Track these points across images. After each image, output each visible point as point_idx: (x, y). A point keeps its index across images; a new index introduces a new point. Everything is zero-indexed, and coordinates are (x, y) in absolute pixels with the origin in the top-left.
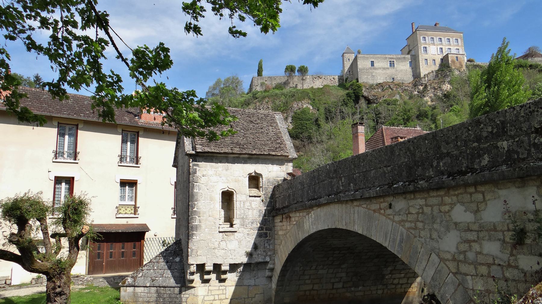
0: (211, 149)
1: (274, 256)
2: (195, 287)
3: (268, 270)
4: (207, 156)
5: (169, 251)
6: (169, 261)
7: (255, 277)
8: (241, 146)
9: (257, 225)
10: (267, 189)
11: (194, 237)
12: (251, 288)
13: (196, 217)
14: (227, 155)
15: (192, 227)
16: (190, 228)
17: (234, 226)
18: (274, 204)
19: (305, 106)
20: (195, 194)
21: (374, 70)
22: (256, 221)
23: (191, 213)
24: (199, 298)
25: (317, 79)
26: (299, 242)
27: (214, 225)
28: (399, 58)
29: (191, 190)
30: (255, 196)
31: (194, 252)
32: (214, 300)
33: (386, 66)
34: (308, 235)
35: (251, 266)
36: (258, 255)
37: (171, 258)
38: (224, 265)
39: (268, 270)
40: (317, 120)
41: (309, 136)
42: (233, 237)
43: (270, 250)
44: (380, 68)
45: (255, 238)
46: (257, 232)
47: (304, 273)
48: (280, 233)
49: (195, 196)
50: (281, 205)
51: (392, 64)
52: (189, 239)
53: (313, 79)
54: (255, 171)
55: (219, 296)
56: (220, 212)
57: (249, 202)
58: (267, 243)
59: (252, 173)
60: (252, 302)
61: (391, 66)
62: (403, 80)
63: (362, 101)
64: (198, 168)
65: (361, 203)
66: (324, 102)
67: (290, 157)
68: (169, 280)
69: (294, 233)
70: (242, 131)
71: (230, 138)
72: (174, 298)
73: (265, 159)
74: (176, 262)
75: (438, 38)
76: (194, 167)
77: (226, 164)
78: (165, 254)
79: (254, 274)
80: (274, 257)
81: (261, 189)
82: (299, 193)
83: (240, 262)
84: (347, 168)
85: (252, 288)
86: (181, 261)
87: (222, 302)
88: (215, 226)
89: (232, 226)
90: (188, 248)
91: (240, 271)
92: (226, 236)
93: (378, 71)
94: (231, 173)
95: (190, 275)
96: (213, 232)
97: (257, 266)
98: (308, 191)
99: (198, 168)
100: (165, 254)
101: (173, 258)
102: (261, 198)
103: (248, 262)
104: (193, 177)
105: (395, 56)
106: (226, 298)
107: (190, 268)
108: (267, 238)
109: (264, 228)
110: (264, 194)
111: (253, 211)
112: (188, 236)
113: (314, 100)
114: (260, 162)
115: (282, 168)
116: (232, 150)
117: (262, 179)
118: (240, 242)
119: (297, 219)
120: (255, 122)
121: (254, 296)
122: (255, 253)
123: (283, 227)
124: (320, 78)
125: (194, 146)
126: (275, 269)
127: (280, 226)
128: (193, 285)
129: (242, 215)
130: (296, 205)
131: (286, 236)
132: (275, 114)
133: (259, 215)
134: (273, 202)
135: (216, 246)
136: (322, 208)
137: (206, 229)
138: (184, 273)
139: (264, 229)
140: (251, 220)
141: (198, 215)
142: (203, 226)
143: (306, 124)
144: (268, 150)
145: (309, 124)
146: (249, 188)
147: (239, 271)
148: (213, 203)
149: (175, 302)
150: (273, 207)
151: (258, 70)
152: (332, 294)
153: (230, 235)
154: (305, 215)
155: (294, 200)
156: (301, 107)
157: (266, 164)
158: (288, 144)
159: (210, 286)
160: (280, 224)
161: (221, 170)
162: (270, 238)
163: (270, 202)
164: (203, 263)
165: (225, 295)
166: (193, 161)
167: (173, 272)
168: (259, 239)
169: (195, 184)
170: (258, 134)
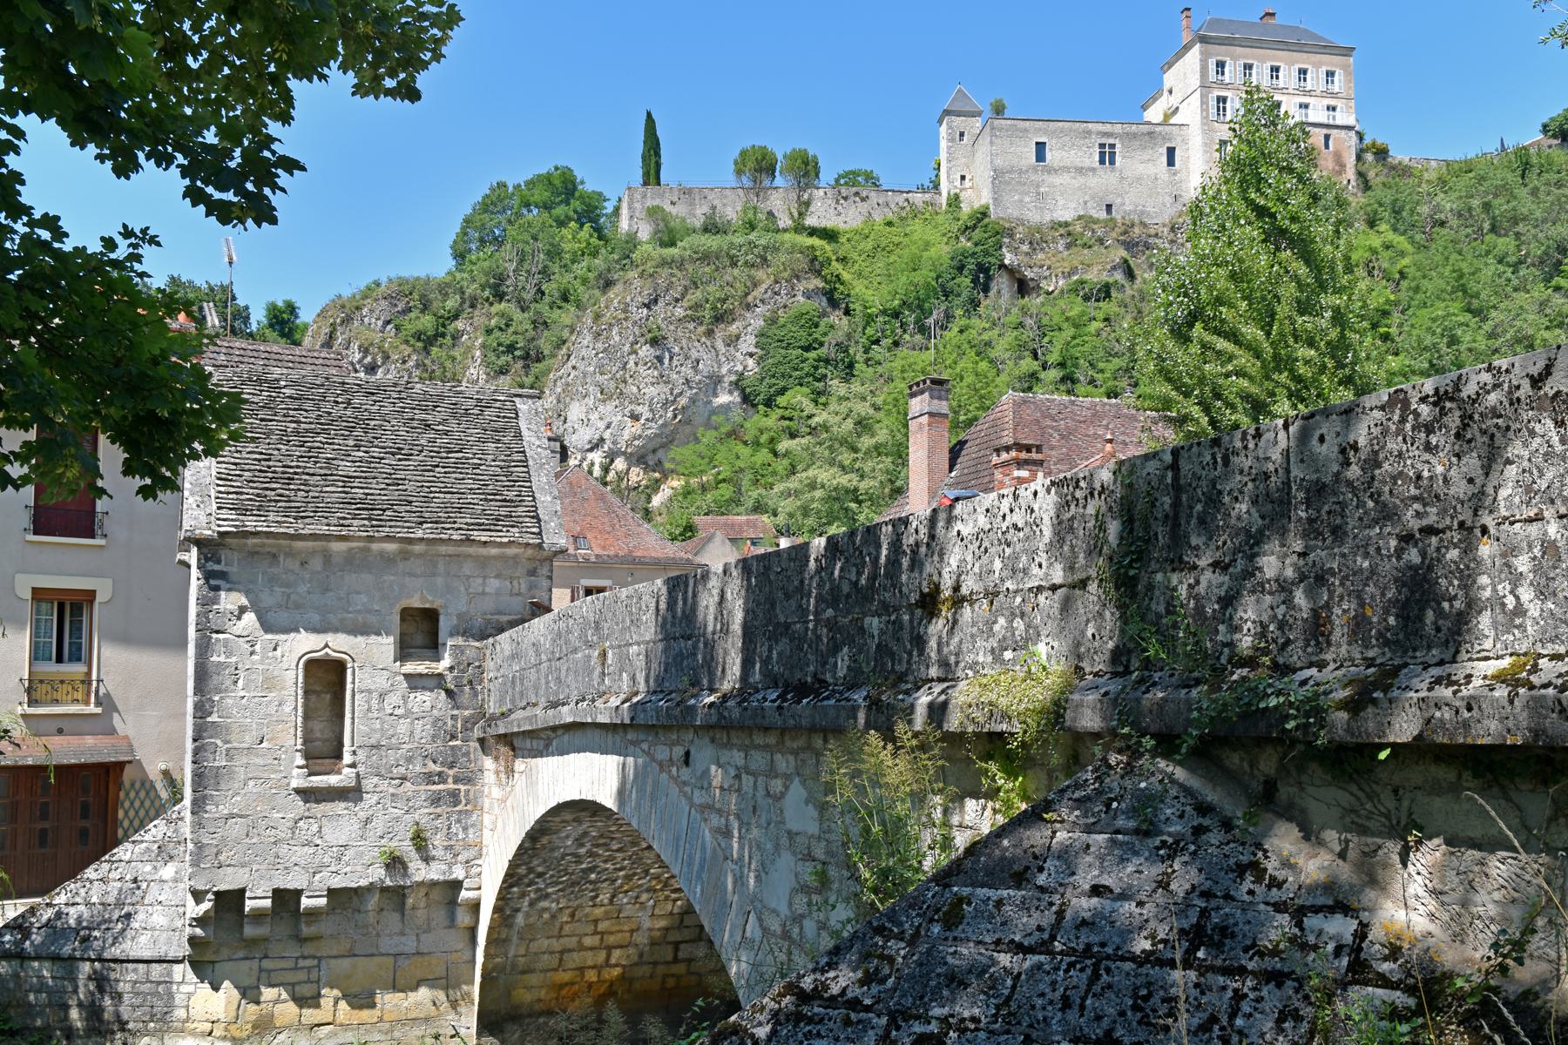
10: (462, 653)
11: (208, 808)
21: (1046, 176)
28: (1135, 136)
33: (1087, 163)
44: (1066, 169)
49: (215, 677)
51: (1107, 156)
58: (459, 821)
61: (1102, 162)
62: (1142, 212)
63: (1001, 283)
65: (642, 737)
75: (1269, 64)
84: (617, 624)
85: (407, 962)
93: (1057, 180)
105: (1118, 129)
109: (448, 776)
124: (863, 200)
132: (517, 400)
136: (571, 733)
139: (450, 780)
152: (673, 975)
162: (469, 807)
165: (315, 985)
168: (431, 810)
169: (214, 636)
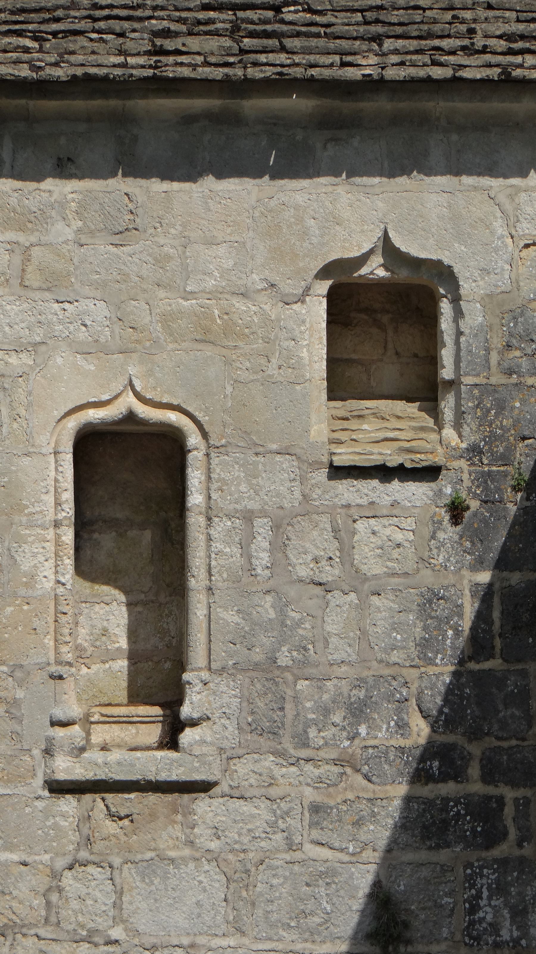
14: (113, 103)
22: (389, 697)
42: (177, 831)
45: (389, 850)
57: (325, 521)
59: (364, 259)
88: (16, 736)
108: (497, 852)
109: (467, 758)
116: (162, 52)
117: (458, 314)
153: (153, 816)
161: (69, 234)
168: (423, 855)
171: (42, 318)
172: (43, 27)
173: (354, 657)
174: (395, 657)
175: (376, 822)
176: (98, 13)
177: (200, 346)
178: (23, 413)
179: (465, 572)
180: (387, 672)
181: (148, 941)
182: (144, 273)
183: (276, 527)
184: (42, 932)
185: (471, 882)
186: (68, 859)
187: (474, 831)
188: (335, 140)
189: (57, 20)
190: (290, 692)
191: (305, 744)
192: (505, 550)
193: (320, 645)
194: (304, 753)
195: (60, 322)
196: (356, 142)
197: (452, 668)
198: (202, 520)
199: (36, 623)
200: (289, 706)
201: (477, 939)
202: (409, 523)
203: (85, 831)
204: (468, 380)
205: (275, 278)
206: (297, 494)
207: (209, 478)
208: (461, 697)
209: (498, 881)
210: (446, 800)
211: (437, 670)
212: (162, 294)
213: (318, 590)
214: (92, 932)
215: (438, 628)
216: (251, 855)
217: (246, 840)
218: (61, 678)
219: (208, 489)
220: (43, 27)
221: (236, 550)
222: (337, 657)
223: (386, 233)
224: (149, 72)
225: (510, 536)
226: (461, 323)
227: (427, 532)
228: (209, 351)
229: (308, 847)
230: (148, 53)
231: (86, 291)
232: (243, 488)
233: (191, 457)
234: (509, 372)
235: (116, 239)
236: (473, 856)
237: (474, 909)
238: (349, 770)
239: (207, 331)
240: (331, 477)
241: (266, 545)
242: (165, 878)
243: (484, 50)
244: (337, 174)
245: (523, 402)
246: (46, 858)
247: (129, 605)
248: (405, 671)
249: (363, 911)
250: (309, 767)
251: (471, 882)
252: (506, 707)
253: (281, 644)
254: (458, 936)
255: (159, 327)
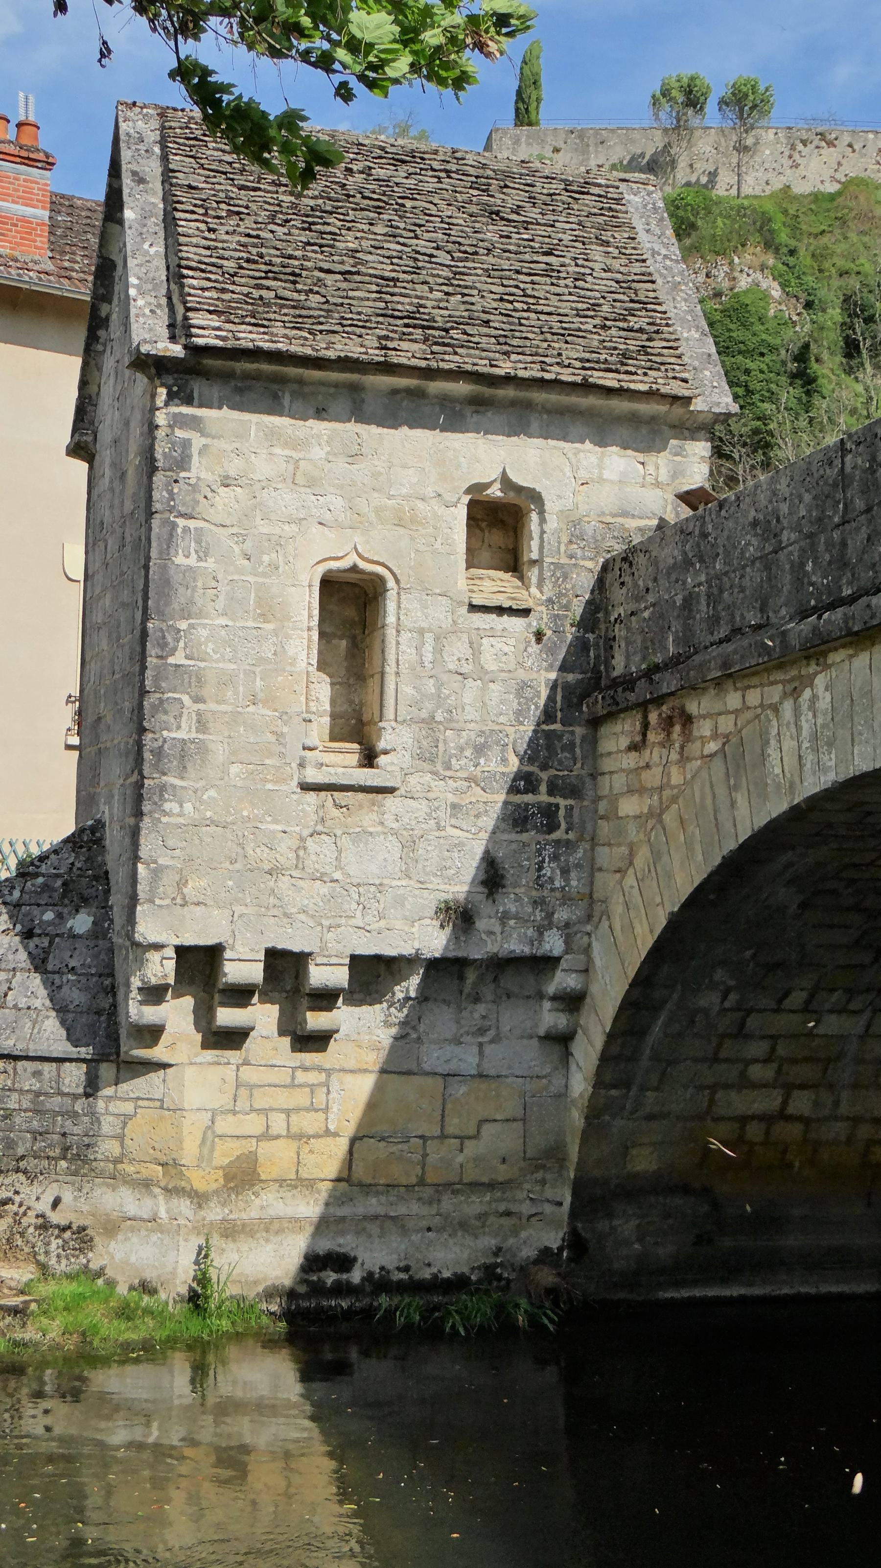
0: (272, 334)
1: (589, 928)
2: (170, 1066)
3: (554, 998)
4: (246, 376)
5: (40, 880)
6: (37, 931)
7: (482, 1031)
8: (436, 333)
9: (504, 760)
10: (565, 577)
11: (167, 806)
12: (460, 1090)
13: (179, 700)
15: (158, 753)
16: (147, 755)
17: (382, 760)
18: (597, 657)
19: (744, 283)
20: (176, 578)
22: (497, 743)
23: (157, 679)
24: (186, 1123)
25: (811, 147)
26: (731, 845)
27: (278, 749)
29: (161, 553)
30: (500, 610)
31: (168, 881)
32: (266, 1136)
34: (784, 806)
35: (462, 978)
36: (504, 918)
37: (49, 916)
38: (325, 960)
39: (554, 998)
40: (802, 355)
41: (756, 432)
42: (374, 816)
43: (567, 899)
45: (494, 833)
46: (501, 797)
47: (742, 1024)
48: (629, 807)
49: (181, 590)
50: (637, 658)
52: (139, 814)
53: (793, 147)
54: (504, 473)
55: (294, 1118)
56: (309, 682)
57: (465, 637)
58: (555, 858)
60: (460, 1159)
64: (197, 441)
66: (840, 263)
67: (698, 405)
68: (35, 1022)
69: (709, 801)
70: (443, 257)
71: (374, 288)
72: (57, 1113)
73: (561, 412)
74: (75, 936)
76: (179, 433)
77: (352, 427)
78: (16, 894)
79: (476, 1015)
80: (589, 934)
81: (533, 575)
82: (746, 582)
83: (407, 950)
85: (463, 1089)
86: (99, 932)
87: (306, 1149)
89: (369, 758)
90: (136, 858)
91: (408, 999)
92: (335, 812)
94: (376, 475)
95: (142, 1003)
96: (269, 786)
97: (495, 980)
98: (802, 565)
99: (197, 441)
100: (16, 894)
101: (60, 916)
102: (533, 621)
103: (450, 955)
104: (168, 484)
106: (328, 1133)
107: (141, 963)
108: (555, 836)
109: (539, 781)
110: (550, 601)
111: (484, 689)
112: (139, 798)
113: (792, 252)
114: (535, 425)
115: (651, 469)
117: (543, 520)
118: (409, 845)
119: (726, 724)
120: (514, 217)
121: (472, 1131)
122: (485, 908)
123: (645, 775)
124: (831, 144)
125: (179, 318)
126: (588, 1000)
127: (629, 772)
128: (158, 1053)
129: (429, 706)
130: (729, 648)
131: (660, 821)
132: (623, 186)
133: (518, 713)
134: (597, 644)
135: (285, 852)
137: (234, 769)
138: (112, 990)
139: (543, 788)
140: (473, 735)
141: (194, 690)
142: (219, 751)
143: (747, 372)
144: (578, 364)
145: (762, 372)
146: (470, 564)
147: (400, 995)
148: (276, 633)
149: (64, 1135)
150: (596, 671)
151: (519, 93)
153: (361, 806)
154: (776, 699)
155: (714, 621)
156: (726, 284)
157: (564, 438)
158: (687, 339)
159: (246, 1063)
160: (631, 760)
162: (571, 836)
163: (580, 646)
164: (210, 942)
165: (321, 1116)
166: (171, 396)
167: (57, 982)
168: (514, 836)
169: (181, 522)
170: (528, 279)
171: (305, 504)
172: (314, 327)
173: (478, 718)
174: (502, 719)
175: (488, 816)
176: (345, 322)
177: (397, 528)
178: (291, 560)
179: (542, 672)
180: (497, 728)
181: (355, 881)
182: (366, 482)
183: (437, 639)
184: (294, 874)
185: (539, 852)
186: (311, 830)
187: (542, 823)
188: (477, 412)
189: (321, 324)
190: (442, 737)
191: (448, 767)
192: (564, 660)
193: (459, 710)
194: (449, 773)
195: (315, 507)
196: (489, 414)
197: (533, 728)
198: (394, 632)
199: (296, 688)
200: (441, 745)
201: (541, 886)
202: (512, 641)
203: (321, 814)
204: (548, 560)
205: (441, 491)
206: (450, 620)
207: (399, 607)
208: (538, 745)
209: (554, 853)
210: (527, 804)
211: (524, 728)
212: (376, 495)
213: (460, 678)
214: (323, 874)
215: (526, 704)
216: (416, 832)
217: (413, 823)
218: (310, 721)
219: (398, 614)
220: (314, 327)
221: (414, 651)
222: (469, 718)
223: (504, 469)
224: (382, 359)
225: (568, 652)
226: (544, 526)
227: (522, 647)
228: (402, 531)
229: (448, 829)
230: (378, 348)
231: (332, 489)
232: (419, 614)
233: (389, 594)
234: (571, 557)
235: (350, 460)
236: (541, 837)
237: (540, 869)
238: (473, 785)
239: (400, 519)
240: (469, 612)
241: (431, 649)
242: (366, 844)
243: (568, 366)
244: (479, 433)
245: (578, 574)
246: (297, 829)
247: (332, 684)
248: (507, 728)
249: (478, 868)
250: (450, 782)
251: (539, 852)
252: (562, 751)
253: (438, 708)
254: (531, 884)
255: (373, 515)
